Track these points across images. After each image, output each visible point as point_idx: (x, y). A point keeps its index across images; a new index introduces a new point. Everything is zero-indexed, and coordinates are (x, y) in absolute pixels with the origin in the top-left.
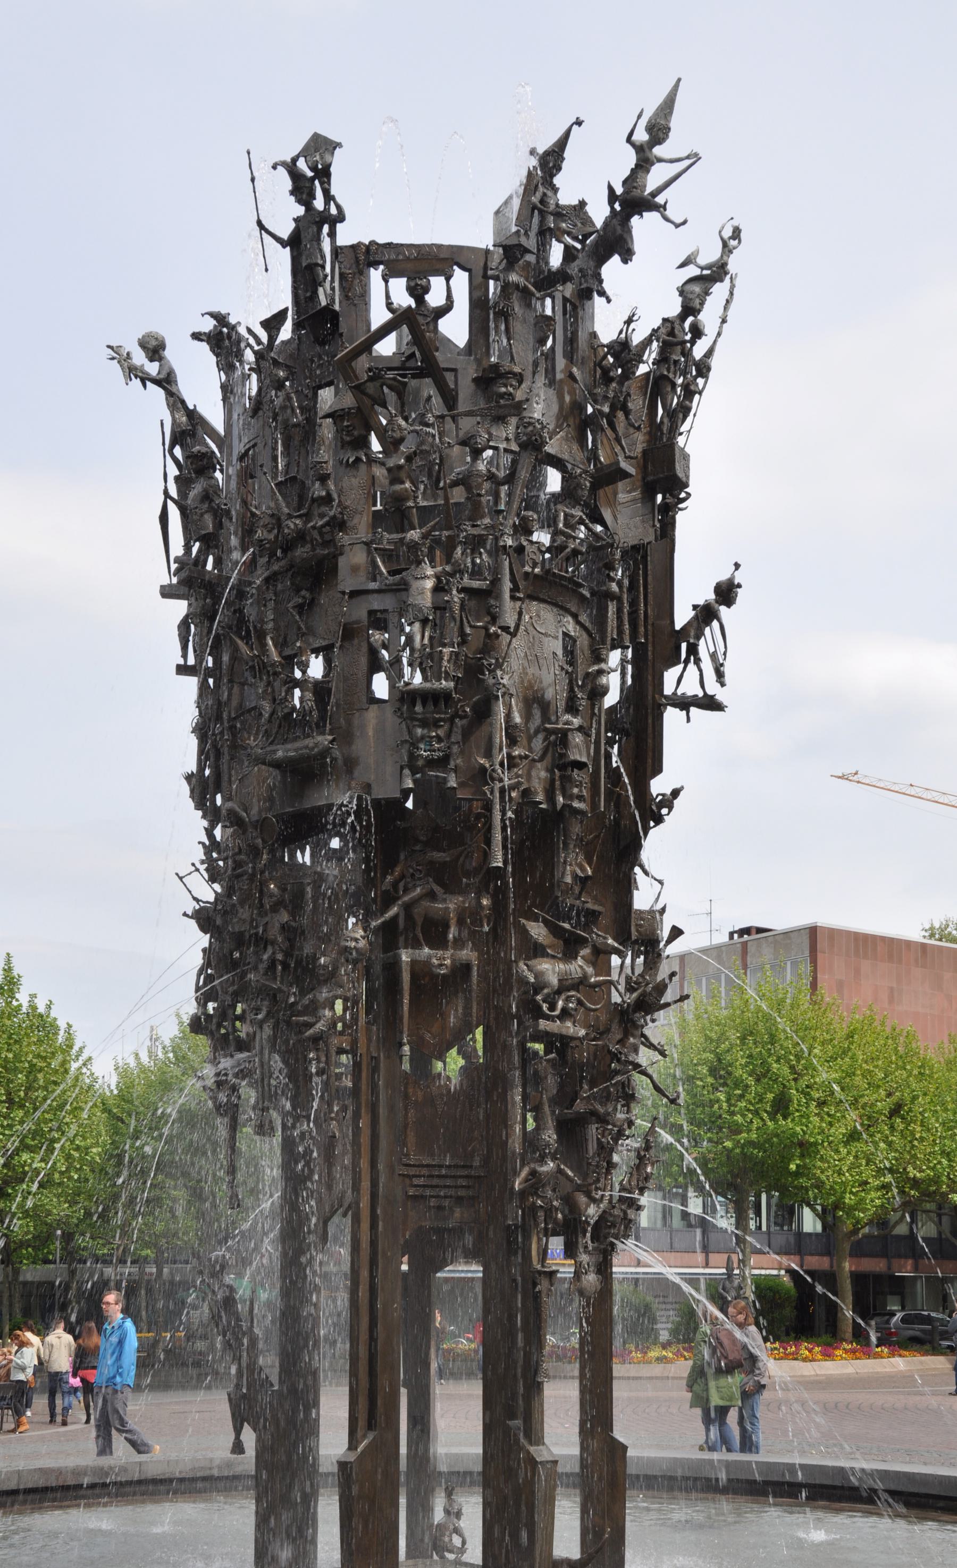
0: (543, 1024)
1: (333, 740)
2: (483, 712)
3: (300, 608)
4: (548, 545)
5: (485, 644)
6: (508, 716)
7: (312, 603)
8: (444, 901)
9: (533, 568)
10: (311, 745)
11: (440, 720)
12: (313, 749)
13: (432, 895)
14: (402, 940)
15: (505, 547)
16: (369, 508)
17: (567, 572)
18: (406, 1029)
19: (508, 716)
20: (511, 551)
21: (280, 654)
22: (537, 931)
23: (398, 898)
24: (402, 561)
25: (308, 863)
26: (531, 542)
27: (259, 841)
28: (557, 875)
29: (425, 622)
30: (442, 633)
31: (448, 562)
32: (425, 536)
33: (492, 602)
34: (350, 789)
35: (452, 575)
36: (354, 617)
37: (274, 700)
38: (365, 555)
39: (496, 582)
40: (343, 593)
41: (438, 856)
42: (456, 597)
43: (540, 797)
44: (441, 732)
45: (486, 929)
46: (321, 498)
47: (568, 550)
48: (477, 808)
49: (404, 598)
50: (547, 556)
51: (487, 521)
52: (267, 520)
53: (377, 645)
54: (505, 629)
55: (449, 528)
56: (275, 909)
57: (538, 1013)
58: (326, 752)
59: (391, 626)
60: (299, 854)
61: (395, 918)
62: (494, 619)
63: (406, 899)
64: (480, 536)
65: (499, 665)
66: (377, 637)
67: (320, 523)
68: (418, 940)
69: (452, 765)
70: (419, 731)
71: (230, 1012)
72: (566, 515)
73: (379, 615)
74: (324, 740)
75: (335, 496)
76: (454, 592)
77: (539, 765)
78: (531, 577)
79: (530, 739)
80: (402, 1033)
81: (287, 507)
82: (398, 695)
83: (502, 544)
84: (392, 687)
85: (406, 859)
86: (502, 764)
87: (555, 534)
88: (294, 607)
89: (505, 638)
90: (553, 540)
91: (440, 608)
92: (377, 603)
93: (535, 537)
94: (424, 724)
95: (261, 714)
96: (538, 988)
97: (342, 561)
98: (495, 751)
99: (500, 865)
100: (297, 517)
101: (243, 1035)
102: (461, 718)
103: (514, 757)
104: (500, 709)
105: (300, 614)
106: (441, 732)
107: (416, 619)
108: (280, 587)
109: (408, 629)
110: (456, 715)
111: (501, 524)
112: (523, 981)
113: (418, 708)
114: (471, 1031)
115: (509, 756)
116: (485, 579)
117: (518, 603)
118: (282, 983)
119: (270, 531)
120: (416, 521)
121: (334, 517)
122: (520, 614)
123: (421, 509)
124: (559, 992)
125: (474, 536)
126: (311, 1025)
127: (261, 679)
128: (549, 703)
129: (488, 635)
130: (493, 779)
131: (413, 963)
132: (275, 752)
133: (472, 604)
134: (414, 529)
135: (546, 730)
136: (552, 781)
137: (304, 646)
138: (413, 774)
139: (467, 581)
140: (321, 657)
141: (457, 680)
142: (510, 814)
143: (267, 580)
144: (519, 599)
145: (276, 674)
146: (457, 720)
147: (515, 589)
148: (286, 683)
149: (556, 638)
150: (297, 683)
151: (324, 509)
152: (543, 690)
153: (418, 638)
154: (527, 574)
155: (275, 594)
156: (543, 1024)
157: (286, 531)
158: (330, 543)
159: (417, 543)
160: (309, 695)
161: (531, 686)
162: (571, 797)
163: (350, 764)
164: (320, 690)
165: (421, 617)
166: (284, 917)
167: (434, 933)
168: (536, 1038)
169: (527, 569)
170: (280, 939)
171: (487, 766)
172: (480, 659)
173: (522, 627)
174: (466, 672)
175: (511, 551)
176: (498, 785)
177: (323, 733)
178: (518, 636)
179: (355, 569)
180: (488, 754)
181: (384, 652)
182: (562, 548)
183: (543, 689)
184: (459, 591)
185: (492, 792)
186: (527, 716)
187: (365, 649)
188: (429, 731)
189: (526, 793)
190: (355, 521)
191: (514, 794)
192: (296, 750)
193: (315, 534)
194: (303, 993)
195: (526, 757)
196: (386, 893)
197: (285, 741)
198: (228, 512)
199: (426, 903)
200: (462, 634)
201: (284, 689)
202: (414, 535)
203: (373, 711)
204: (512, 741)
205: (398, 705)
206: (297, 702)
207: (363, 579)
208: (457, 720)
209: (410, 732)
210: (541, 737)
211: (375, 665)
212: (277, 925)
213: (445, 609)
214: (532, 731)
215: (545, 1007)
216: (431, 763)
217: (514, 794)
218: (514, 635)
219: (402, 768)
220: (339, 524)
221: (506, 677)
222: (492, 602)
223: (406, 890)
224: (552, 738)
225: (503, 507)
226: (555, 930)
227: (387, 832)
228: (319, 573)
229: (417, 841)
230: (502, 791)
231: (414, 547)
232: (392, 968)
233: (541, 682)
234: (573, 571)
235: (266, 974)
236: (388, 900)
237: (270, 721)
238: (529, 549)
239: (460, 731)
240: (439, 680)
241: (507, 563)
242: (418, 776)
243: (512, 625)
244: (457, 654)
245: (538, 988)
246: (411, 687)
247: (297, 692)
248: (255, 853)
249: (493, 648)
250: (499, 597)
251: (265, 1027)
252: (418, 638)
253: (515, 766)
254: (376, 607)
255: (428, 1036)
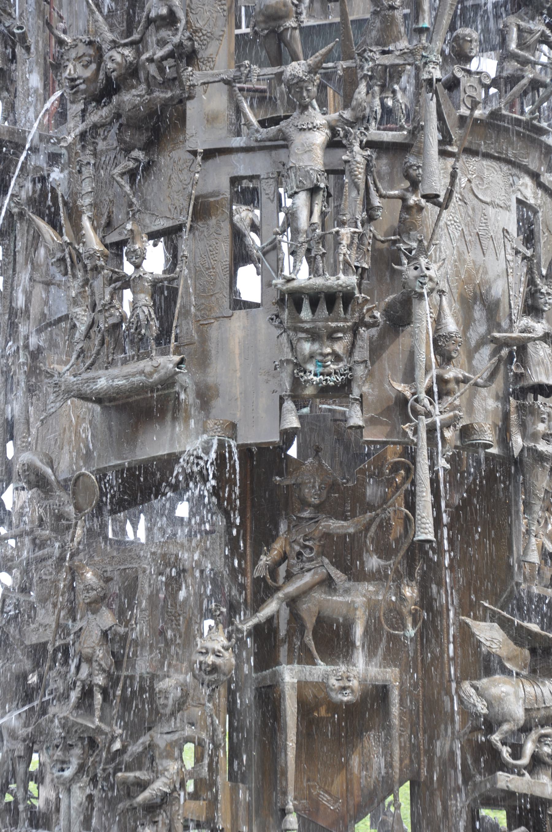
0: (504, 780)
1: (182, 361)
2: (400, 317)
3: (132, 175)
4: (493, 75)
5: (402, 221)
6: (438, 321)
7: (148, 167)
8: (347, 591)
9: (472, 109)
10: (148, 369)
11: (338, 330)
12: (151, 374)
13: (328, 583)
14: (283, 651)
15: (430, 82)
16: (231, 32)
17: (522, 113)
18: (291, 787)
19: (438, 321)
20: (439, 87)
21: (103, 240)
22: (490, 635)
23: (278, 589)
24: (279, 107)
25: (143, 540)
26: (469, 72)
27: (71, 509)
28: (517, 548)
29: (313, 191)
30: (338, 207)
31: (346, 106)
32: (313, 70)
33: (412, 160)
34: (205, 431)
35: (352, 124)
36: (210, 188)
37: (94, 307)
38: (224, 98)
39: (417, 130)
40: (194, 153)
41: (335, 525)
42: (358, 156)
43: (489, 436)
44: (339, 347)
45: (411, 632)
46: (161, 18)
47: (525, 81)
48: (393, 456)
49: (284, 159)
50: (493, 91)
51: (403, 44)
52: (82, 49)
53: (244, 227)
54: (431, 198)
55: (349, 56)
56: (94, 606)
57: (496, 763)
58: (169, 382)
59: (264, 198)
60: (129, 527)
61: (270, 620)
62: (415, 184)
63: (291, 589)
64: (394, 66)
65: (423, 250)
66: (244, 214)
67: (160, 54)
68: (308, 651)
69: (356, 393)
70: (307, 347)
71: (20, 769)
72: (520, 30)
73: (245, 183)
74: (167, 362)
75: (181, 14)
76: (357, 148)
77: (484, 391)
78: (470, 122)
79: (470, 358)
80: (285, 793)
81: (111, 31)
82: (276, 296)
83: (425, 76)
84: (266, 285)
85: (289, 530)
86: (429, 392)
87: (506, 57)
88: (122, 175)
89: (431, 209)
90: (500, 67)
91: (335, 172)
92: (242, 166)
93: (473, 66)
94: (314, 336)
95: (74, 326)
96: (490, 725)
97: (191, 107)
98: (420, 373)
99: (431, 537)
100: (125, 45)
101: (39, 804)
102: (368, 326)
103: (447, 382)
104: (424, 312)
105: (132, 181)
106: (339, 347)
107: (301, 188)
108: (101, 145)
109: (288, 202)
110: (361, 323)
111: (424, 48)
112: (467, 712)
113: (306, 314)
114: (391, 790)
115: (441, 380)
116: (402, 128)
117: (451, 161)
118: (101, 719)
119: (86, 66)
120: (299, 48)
121: (180, 45)
122: (453, 176)
123: (308, 33)
124: (526, 729)
125: (385, 67)
126: (143, 785)
127: (74, 276)
128: (497, 303)
129: (407, 208)
130: (416, 413)
131: (302, 686)
132: (94, 380)
133: (383, 165)
134: (295, 58)
135: (494, 340)
136: (506, 416)
137: (136, 228)
138: (299, 407)
139: (375, 133)
140: (161, 245)
141: (362, 273)
142: (442, 463)
143: (83, 135)
144: (451, 155)
145: (96, 269)
146: (362, 330)
147: (446, 139)
148: (111, 281)
149: (508, 208)
150: (127, 282)
151: (164, 33)
152: (489, 284)
153: (303, 215)
154: (462, 119)
155: (95, 154)
156: (504, 780)
157: (110, 65)
158: (175, 81)
159: (301, 80)
160: (145, 299)
161: (470, 279)
162: (535, 437)
163: (205, 397)
164: (164, 293)
165: (309, 185)
166: (107, 619)
167: (333, 640)
168: (491, 802)
169: (464, 111)
170: (100, 653)
171: (408, 394)
172: (395, 242)
173: (456, 195)
174: (374, 260)
175: (439, 87)
176: (424, 422)
177: (164, 353)
178: (451, 208)
179: (211, 119)
180: (409, 377)
181: (253, 235)
182: (513, 80)
183: (487, 282)
184: (362, 147)
185: (416, 432)
186: (467, 322)
187: (226, 230)
188: (322, 345)
189: (466, 432)
190: (211, 50)
191: (448, 434)
192: (126, 377)
193: (152, 69)
194: (134, 731)
195: (465, 380)
196: (258, 581)
197: (111, 364)
198: (23, 38)
199: (319, 596)
200: (368, 206)
201: (108, 290)
202: (296, 68)
203: (239, 321)
204: (445, 358)
205: (275, 309)
206: (127, 309)
207: (223, 133)
208: (362, 330)
209: (293, 349)
210: (486, 351)
211: (241, 256)
212: (97, 633)
213: (343, 172)
214: (473, 343)
215: (505, 752)
216: (324, 392)
217: (448, 434)
218: (444, 206)
219: (282, 400)
220: (188, 56)
221: (434, 267)
222: (412, 160)
223: (289, 576)
224: (505, 352)
225: (426, 23)
226: (519, 636)
227: (258, 488)
228: (158, 127)
229: (305, 504)
230: (431, 430)
231: (297, 85)
232: (269, 698)
233: (486, 273)
234: (532, 112)
235: (78, 706)
236: (263, 590)
237: (87, 336)
238: (465, 81)
239: (366, 345)
240: (334, 273)
241: (433, 104)
242: (306, 410)
243: (442, 194)
244: (361, 236)
245: (490, 725)
246: (294, 284)
247: (128, 294)
248: (60, 524)
249: (413, 227)
250: (421, 153)
251: (75, 789)
252: (303, 215)
253: (449, 393)
254: (242, 172)
255: (325, 799)
